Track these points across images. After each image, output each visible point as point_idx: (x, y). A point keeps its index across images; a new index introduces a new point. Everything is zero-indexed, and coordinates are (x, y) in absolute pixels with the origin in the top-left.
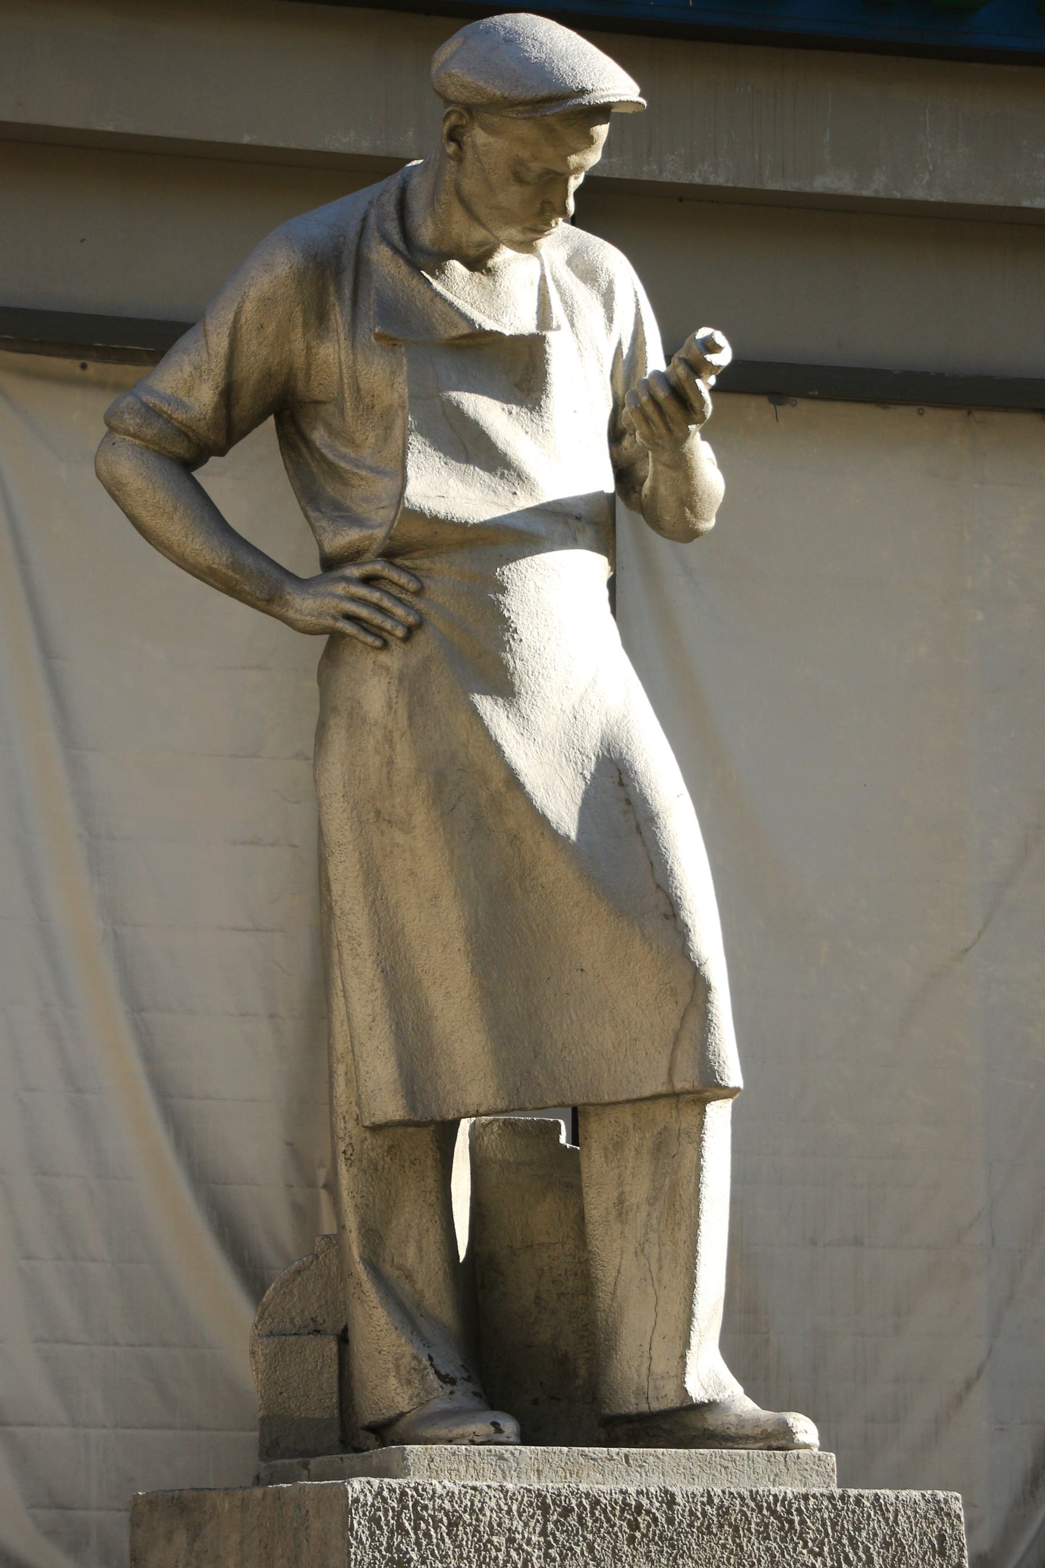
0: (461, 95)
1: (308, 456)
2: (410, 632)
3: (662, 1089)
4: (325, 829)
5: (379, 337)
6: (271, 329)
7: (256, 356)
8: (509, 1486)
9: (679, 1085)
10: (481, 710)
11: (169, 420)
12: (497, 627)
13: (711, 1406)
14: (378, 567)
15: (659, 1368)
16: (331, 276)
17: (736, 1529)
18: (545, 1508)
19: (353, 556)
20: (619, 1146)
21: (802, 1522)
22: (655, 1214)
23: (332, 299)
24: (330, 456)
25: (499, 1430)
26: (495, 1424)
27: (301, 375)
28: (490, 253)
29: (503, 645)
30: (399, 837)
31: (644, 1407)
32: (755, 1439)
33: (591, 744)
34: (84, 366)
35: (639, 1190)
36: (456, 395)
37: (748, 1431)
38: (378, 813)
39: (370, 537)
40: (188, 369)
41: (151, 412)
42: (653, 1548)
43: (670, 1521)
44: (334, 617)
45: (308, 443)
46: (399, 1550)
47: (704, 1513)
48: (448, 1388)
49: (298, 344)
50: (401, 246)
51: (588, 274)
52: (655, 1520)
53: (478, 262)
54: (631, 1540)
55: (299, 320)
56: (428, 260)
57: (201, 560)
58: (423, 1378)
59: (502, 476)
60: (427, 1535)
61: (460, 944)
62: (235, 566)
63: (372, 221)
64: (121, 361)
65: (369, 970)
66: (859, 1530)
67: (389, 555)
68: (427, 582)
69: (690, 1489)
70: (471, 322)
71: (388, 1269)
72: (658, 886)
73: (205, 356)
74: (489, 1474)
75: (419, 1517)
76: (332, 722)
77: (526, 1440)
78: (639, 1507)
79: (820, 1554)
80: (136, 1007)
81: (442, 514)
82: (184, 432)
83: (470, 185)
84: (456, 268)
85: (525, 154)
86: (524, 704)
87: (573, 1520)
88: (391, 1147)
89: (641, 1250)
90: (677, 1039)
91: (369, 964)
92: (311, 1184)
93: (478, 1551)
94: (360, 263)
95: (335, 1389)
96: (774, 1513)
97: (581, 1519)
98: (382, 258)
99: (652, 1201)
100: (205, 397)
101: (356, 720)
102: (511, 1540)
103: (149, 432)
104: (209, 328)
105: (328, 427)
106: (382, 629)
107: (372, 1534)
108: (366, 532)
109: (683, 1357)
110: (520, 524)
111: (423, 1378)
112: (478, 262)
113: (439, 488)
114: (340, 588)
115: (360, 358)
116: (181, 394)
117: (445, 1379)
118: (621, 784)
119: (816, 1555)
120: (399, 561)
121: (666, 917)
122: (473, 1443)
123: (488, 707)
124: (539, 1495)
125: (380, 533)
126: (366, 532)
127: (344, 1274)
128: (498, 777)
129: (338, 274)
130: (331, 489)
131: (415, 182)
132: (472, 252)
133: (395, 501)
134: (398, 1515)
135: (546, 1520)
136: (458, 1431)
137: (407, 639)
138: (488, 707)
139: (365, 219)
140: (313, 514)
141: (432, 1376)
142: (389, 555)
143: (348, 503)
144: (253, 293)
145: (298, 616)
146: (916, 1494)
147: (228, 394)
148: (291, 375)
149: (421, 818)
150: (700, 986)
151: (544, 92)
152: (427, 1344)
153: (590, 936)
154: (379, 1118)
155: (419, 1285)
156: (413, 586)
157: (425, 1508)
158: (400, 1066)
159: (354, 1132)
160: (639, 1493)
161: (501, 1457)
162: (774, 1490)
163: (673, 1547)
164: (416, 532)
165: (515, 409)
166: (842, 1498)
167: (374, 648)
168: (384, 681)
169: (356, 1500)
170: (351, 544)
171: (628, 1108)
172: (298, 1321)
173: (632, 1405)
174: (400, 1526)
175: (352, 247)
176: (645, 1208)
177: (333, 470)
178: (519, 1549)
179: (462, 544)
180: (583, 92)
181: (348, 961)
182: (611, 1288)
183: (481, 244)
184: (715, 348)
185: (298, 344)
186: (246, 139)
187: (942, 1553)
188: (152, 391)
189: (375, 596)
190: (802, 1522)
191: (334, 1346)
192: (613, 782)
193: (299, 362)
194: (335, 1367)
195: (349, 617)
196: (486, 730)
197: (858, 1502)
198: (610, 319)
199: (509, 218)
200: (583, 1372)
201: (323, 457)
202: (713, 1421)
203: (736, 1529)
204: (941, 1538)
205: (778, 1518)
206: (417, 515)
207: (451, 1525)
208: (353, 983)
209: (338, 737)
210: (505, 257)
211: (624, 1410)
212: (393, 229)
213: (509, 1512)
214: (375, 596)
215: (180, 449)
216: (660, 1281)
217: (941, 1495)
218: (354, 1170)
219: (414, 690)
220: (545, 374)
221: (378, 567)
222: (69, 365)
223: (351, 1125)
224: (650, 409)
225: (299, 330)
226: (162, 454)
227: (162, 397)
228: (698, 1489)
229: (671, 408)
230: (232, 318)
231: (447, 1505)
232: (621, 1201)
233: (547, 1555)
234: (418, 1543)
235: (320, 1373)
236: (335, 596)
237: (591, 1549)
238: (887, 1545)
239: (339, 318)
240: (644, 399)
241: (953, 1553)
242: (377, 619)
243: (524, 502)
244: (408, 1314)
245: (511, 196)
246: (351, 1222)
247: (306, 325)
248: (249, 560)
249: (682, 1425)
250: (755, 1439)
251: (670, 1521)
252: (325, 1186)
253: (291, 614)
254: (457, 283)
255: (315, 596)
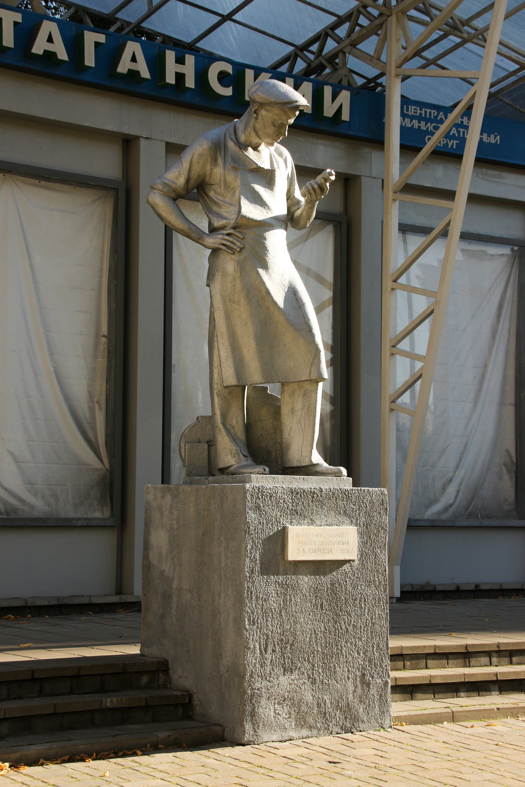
0: (261, 100)
1: (208, 200)
2: (241, 249)
3: (308, 379)
4: (214, 303)
5: (232, 167)
6: (201, 163)
7: (197, 170)
8: (284, 486)
9: (312, 378)
10: (260, 272)
11: (171, 187)
12: (264, 249)
13: (317, 465)
14: (231, 231)
15: (304, 454)
16: (218, 148)
17: (336, 498)
18: (292, 492)
19: (223, 228)
20: (293, 394)
21: (351, 496)
22: (303, 413)
23: (219, 156)
24: (216, 200)
25: (265, 471)
26: (264, 469)
27: (208, 177)
28: (258, 146)
29: (266, 255)
30: (237, 307)
31: (299, 465)
32: (331, 474)
33: (287, 284)
34: (40, 182)
35: (299, 406)
36: (253, 185)
37: (329, 471)
38: (230, 300)
39: (229, 223)
40: (177, 173)
41: (166, 184)
42: (317, 503)
43: (321, 496)
44: (219, 244)
45: (208, 196)
46: (258, 503)
47: (329, 494)
48: (246, 459)
49: (208, 168)
50: (236, 143)
51: (280, 155)
52: (318, 496)
53: (256, 148)
54: (312, 501)
55: (209, 161)
56: (244, 147)
57: (180, 227)
58: (239, 456)
59: (264, 208)
60: (265, 499)
61: (253, 337)
62: (190, 229)
63: (227, 135)
64: (49, 181)
65: (227, 343)
66: (364, 498)
67: (234, 228)
68: (246, 236)
69: (326, 488)
70: (257, 165)
71: (227, 426)
72: (306, 323)
73: (182, 169)
74: (271, 483)
75: (263, 495)
76: (217, 274)
77: (271, 473)
78: (314, 492)
79: (355, 505)
80: (51, 354)
81: (251, 218)
82: (174, 191)
83: (258, 126)
84: (250, 149)
85: (277, 118)
86: (270, 271)
87: (299, 496)
88: (230, 392)
89: (298, 422)
90: (312, 365)
91: (227, 341)
92: (93, 402)
93: (276, 504)
94: (225, 146)
95: (207, 458)
96: (345, 494)
97: (301, 495)
98: (231, 145)
99: (302, 409)
100: (182, 181)
101: (225, 274)
102: (284, 501)
103: (165, 190)
104: (183, 162)
105: (216, 192)
106: (232, 248)
107: (251, 499)
108: (228, 221)
109: (311, 451)
110: (269, 221)
111: (239, 456)
112: (256, 148)
113: (250, 210)
114: (220, 236)
115: (227, 173)
116: (175, 180)
117: (245, 456)
118: (295, 294)
119: (354, 505)
120: (237, 230)
121: (309, 331)
122: (258, 474)
123: (261, 271)
124: (291, 489)
125: (232, 222)
126: (228, 221)
127: (214, 427)
128: (264, 291)
129: (220, 149)
130: (215, 208)
131: (238, 125)
132: (254, 145)
133: (237, 213)
134: (258, 494)
135: (293, 496)
136: (254, 470)
137: (240, 252)
138: (261, 271)
139: (225, 134)
140: (210, 216)
141: (241, 455)
142: (234, 228)
143: (221, 213)
144: (196, 152)
145: (207, 244)
146: (377, 489)
147: (188, 180)
148: (205, 176)
149: (243, 301)
150: (318, 351)
151: (286, 101)
152: (239, 447)
153: (288, 337)
154: (229, 384)
155: (236, 430)
156: (241, 237)
157: (264, 492)
158: (235, 369)
159: (220, 388)
160: (314, 488)
161: (274, 478)
162: (345, 488)
163: (322, 503)
164: (244, 222)
165: (267, 190)
166: (360, 490)
167: (230, 253)
168: (233, 263)
169: (248, 490)
170: (223, 225)
171: (296, 383)
172: (194, 439)
173: (295, 464)
174: (258, 497)
175: (223, 142)
176: (300, 411)
177: (216, 203)
178: (286, 503)
179: (255, 226)
180: (297, 101)
181: (220, 341)
182: (288, 432)
183: (257, 143)
184: (332, 175)
185: (208, 168)
186: (86, 125)
187: (383, 505)
188: (165, 178)
189: (231, 239)
190: (351, 496)
191: (206, 446)
192: (292, 293)
193: (208, 173)
194: (207, 452)
195: (223, 244)
196: (261, 278)
197: (364, 491)
198: (287, 167)
199: (268, 136)
200: (274, 455)
201: (213, 200)
202: (318, 469)
203: (336, 498)
204: (383, 501)
205: (346, 495)
206: (244, 217)
207: (270, 497)
208: (221, 347)
209: (218, 277)
210: (263, 147)
211: (293, 465)
212: (233, 137)
213: (284, 493)
214: (231, 239)
215: (173, 195)
216: (305, 431)
217: (382, 489)
218: (219, 398)
219: (241, 267)
220: (275, 180)
221: (231, 231)
222: (36, 181)
223: (219, 386)
224: (312, 191)
225: (209, 164)
226: (168, 197)
227: (169, 181)
228: (327, 487)
229: (318, 191)
230: (190, 159)
231: (269, 491)
232: (293, 409)
233: (293, 505)
234: (262, 502)
235: (203, 453)
236: (219, 238)
237: (303, 504)
238: (370, 503)
239: (220, 161)
240: (310, 188)
241: (385, 505)
242: (232, 246)
243: (270, 215)
244: (233, 438)
245: (271, 130)
246: (218, 412)
247: (211, 162)
248: (193, 227)
249: (308, 470)
250: (331, 474)
251: (321, 496)
252: (97, 402)
253: (205, 243)
254: (250, 153)
255: (213, 238)
